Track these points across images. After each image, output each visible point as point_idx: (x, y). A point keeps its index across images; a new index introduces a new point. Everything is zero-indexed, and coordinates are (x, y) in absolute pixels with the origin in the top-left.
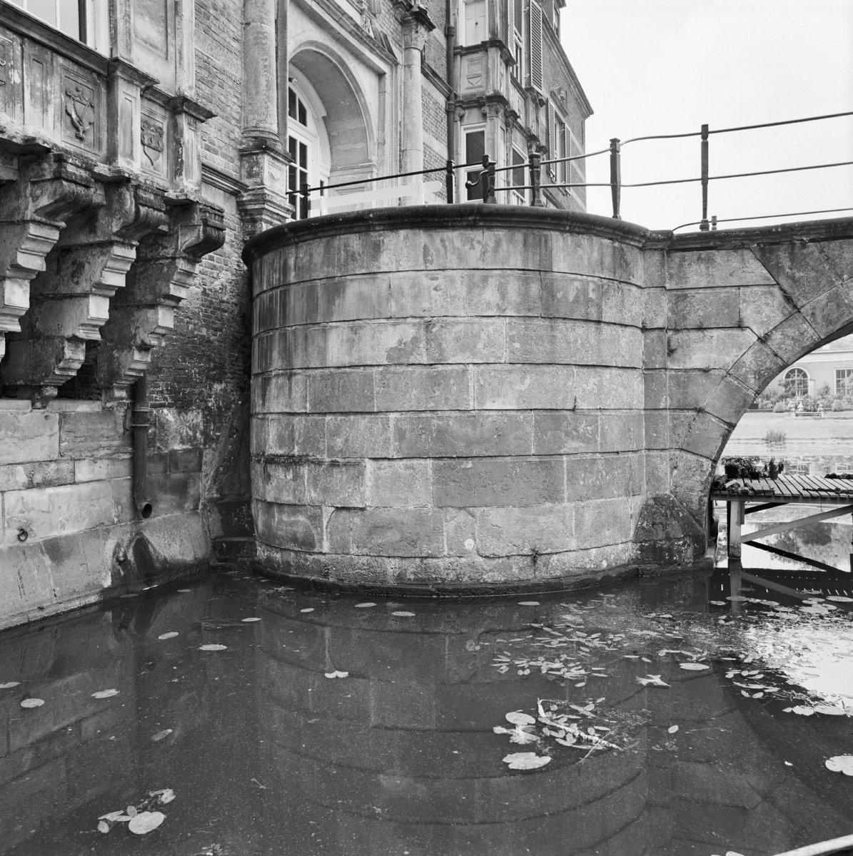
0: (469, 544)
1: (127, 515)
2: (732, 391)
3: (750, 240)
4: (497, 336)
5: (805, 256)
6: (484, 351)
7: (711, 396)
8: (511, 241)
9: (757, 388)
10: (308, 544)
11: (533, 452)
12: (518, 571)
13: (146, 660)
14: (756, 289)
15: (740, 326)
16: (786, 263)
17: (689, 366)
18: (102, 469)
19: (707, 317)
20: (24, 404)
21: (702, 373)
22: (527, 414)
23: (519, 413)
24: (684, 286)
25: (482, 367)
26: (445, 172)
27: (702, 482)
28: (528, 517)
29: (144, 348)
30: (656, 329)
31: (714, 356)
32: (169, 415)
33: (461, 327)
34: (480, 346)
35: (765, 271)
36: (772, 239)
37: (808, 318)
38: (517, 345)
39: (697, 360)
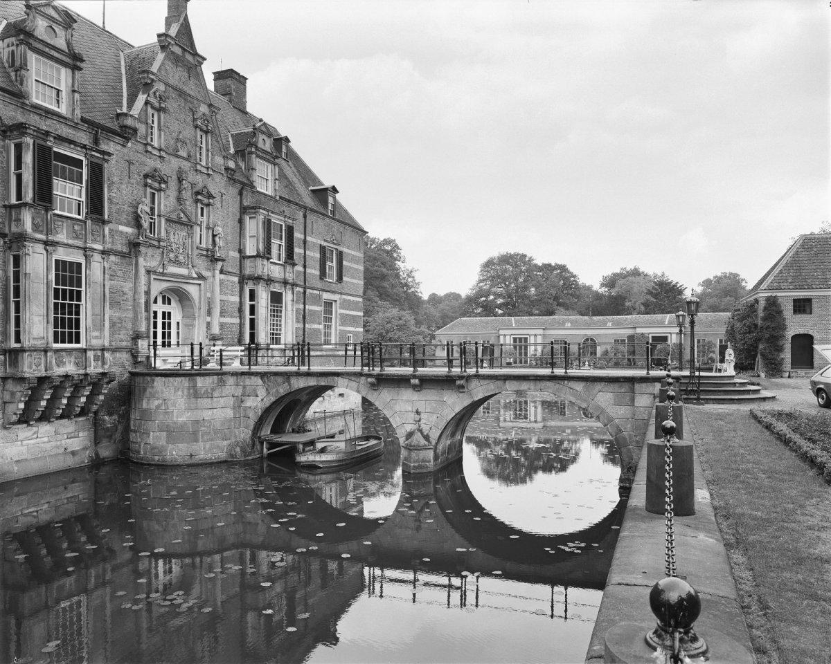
0: (174, 453)
1: (93, 444)
10: (138, 452)
13: (97, 483)
15: (257, 396)
18: (86, 433)
20: (66, 420)
29: (96, 404)
32: (106, 418)
39: (248, 404)
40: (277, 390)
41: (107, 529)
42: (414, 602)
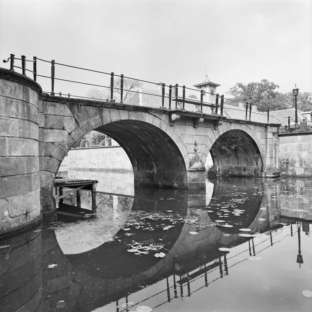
2: (61, 150)
3: (67, 102)
4: (15, 126)
5: (81, 109)
6: (11, 132)
7: (55, 152)
8: (19, 88)
9: (68, 149)
11: (26, 173)
12: (23, 221)
14: (68, 117)
15: (63, 129)
16: (76, 111)
17: (48, 141)
19: (54, 125)
21: (52, 144)
22: (24, 157)
23: (21, 157)
24: (46, 113)
25: (10, 138)
26: (185, 104)
27: (52, 181)
28: (25, 198)
30: (41, 127)
31: (56, 138)
33: (3, 120)
34: (10, 129)
35: (71, 112)
36: (73, 102)
37: (81, 128)
38: (21, 130)
39: (50, 139)
40: (88, 123)
41: (212, 211)
42: (292, 235)
